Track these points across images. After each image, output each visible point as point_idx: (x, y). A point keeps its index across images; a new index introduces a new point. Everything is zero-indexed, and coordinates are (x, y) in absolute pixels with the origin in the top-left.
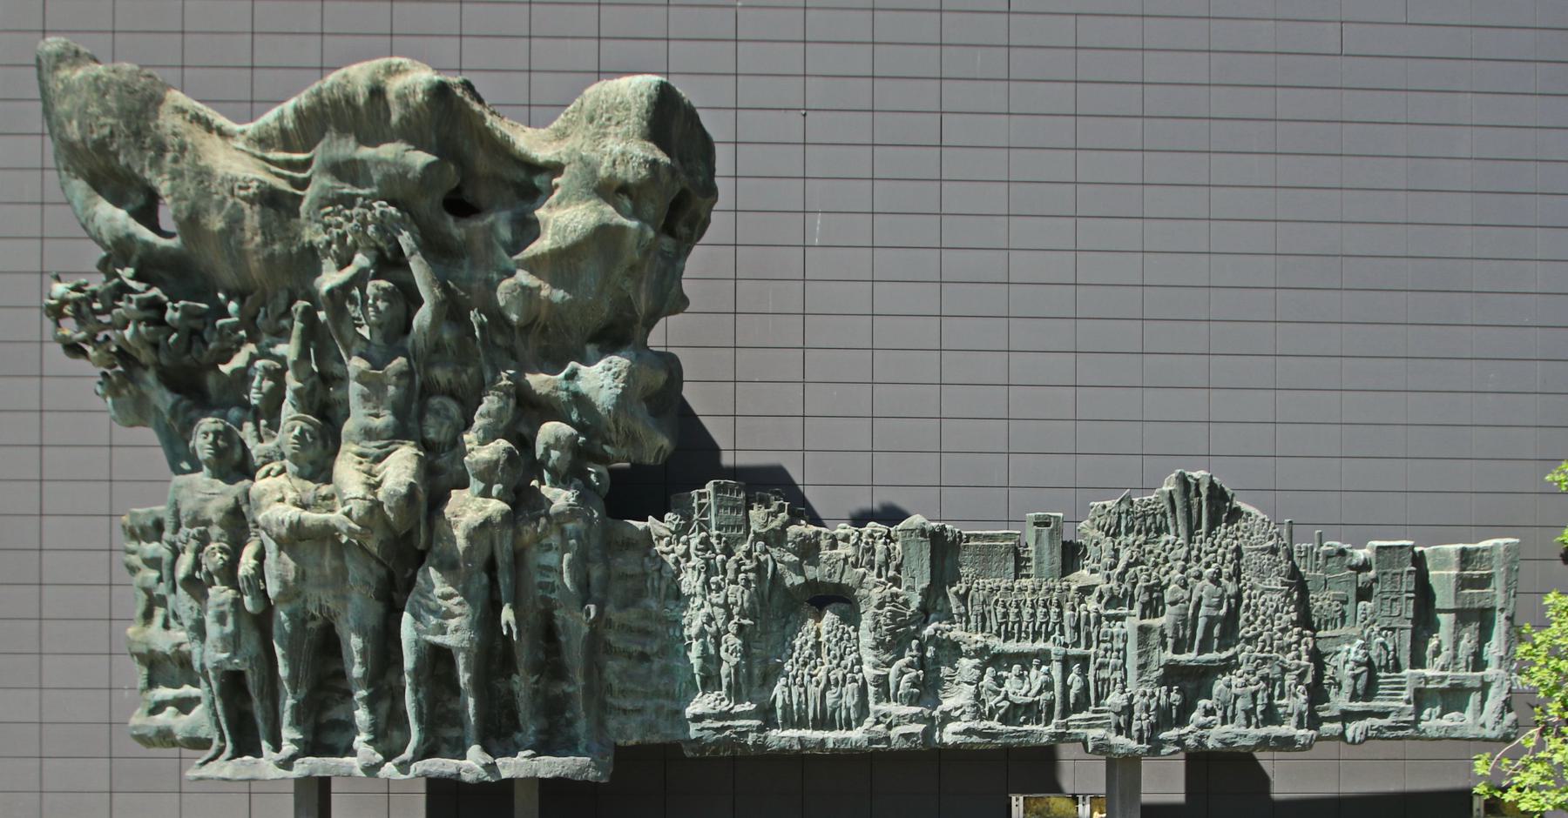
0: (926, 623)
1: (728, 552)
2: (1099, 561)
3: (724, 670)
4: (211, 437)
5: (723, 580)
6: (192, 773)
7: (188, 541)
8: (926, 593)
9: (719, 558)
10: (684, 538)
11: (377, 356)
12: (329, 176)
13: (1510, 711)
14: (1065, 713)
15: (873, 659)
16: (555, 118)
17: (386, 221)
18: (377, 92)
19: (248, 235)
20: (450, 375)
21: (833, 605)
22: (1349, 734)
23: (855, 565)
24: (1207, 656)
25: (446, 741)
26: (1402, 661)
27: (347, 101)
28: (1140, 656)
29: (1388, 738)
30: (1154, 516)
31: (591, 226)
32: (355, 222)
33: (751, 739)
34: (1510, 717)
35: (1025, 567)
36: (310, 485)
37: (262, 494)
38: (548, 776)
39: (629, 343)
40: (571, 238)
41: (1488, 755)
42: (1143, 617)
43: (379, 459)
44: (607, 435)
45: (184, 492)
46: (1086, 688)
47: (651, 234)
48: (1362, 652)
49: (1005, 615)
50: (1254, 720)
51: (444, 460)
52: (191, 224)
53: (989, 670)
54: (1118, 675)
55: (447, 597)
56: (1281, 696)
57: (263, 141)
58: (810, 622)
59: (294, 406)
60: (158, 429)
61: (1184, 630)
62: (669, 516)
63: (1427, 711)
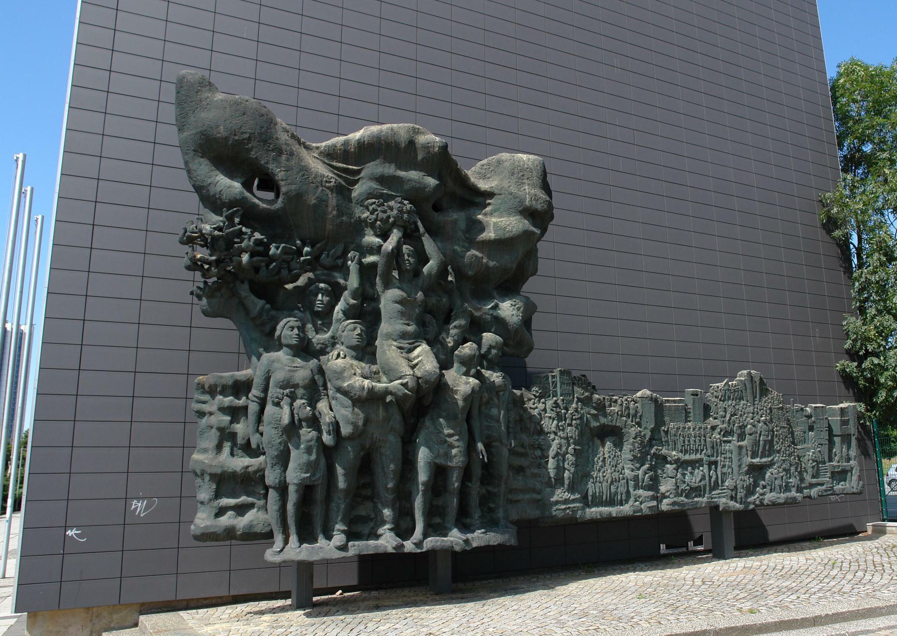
0: (651, 446)
1: (567, 409)
2: (717, 414)
3: (566, 474)
7: (283, 398)
8: (652, 431)
10: (543, 400)
12: (375, 182)
14: (711, 490)
16: (474, 165)
19: (330, 209)
23: (622, 416)
27: (395, 144)
31: (521, 231)
34: (861, 483)
38: (495, 544)
43: (410, 351)
45: (276, 365)
50: (782, 490)
55: (450, 436)
62: (535, 389)
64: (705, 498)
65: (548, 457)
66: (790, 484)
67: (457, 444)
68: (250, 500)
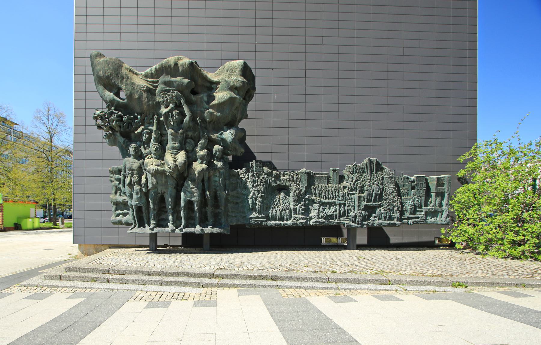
0: (306, 195)
1: (259, 178)
2: (348, 180)
3: (257, 206)
4: (134, 149)
5: (257, 184)
6: (129, 231)
8: (306, 188)
9: (256, 179)
10: (247, 174)
11: (176, 129)
13: (448, 217)
14: (339, 217)
15: (293, 204)
17: (178, 96)
18: (176, 64)
19: (144, 99)
20: (192, 134)
21: (283, 191)
22: (409, 223)
23: (289, 181)
24: (375, 203)
25: (190, 223)
26: (422, 205)
27: (169, 66)
28: (358, 203)
29: (419, 224)
30: (362, 169)
32: (170, 96)
33: (263, 223)
35: (330, 181)
36: (158, 161)
37: (148, 163)
39: (234, 126)
40: (223, 100)
41: (444, 228)
42: (359, 194)
43: (176, 154)
44: (229, 148)
46: (345, 211)
47: (242, 99)
48: (413, 202)
49: (325, 193)
50: (386, 219)
51: (190, 155)
52: (130, 96)
53: (321, 207)
54: (353, 208)
56: (393, 213)
57: (146, 76)
58: (278, 196)
59: (154, 141)
60: (119, 147)
61: (370, 197)
63: (428, 217)
64: (336, 220)
65: (249, 198)
66: (393, 217)
67: (195, 191)
68: (127, 211)
